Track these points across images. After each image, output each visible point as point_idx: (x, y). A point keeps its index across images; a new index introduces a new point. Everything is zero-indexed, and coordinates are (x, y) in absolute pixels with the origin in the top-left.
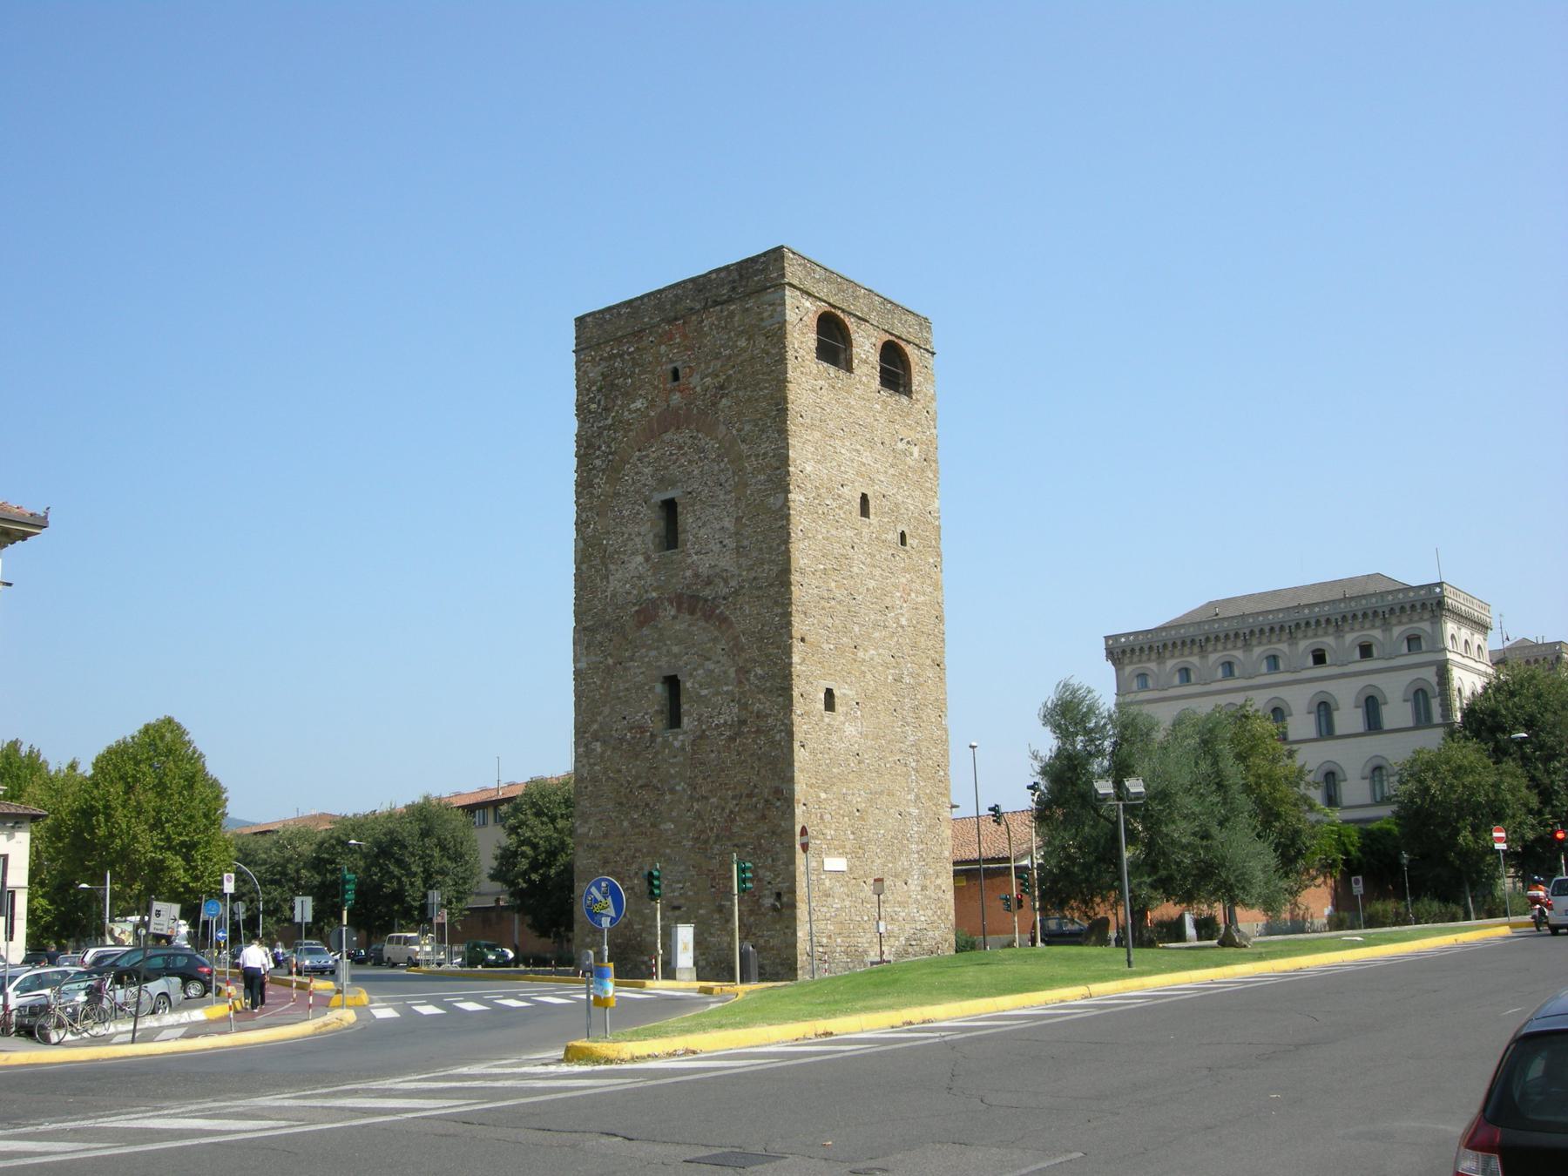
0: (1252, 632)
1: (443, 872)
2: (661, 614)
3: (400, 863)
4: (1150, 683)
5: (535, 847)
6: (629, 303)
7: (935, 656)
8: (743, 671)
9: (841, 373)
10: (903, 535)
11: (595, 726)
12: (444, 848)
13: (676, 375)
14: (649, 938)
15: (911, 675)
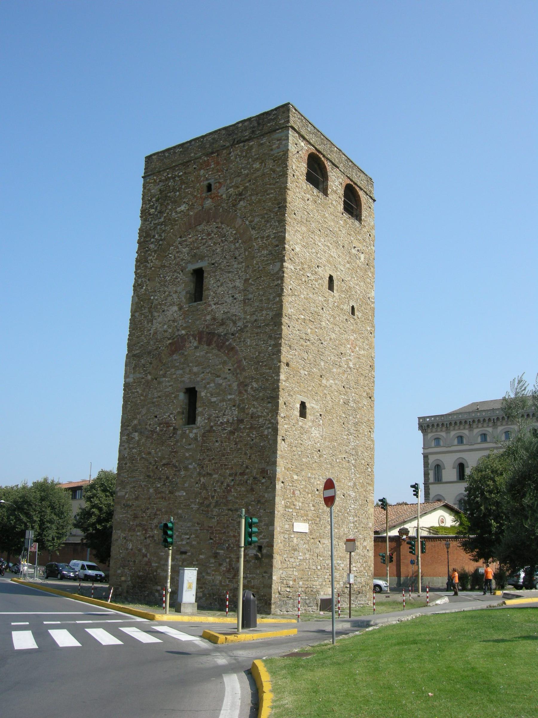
0: (498, 419)
1: (51, 522)
2: (187, 345)
3: (27, 515)
4: (441, 443)
5: (100, 509)
6: (181, 145)
7: (369, 391)
8: (243, 385)
9: (321, 195)
10: (353, 308)
11: (135, 422)
12: (53, 508)
13: (209, 188)
14: (162, 574)
15: (354, 401)
